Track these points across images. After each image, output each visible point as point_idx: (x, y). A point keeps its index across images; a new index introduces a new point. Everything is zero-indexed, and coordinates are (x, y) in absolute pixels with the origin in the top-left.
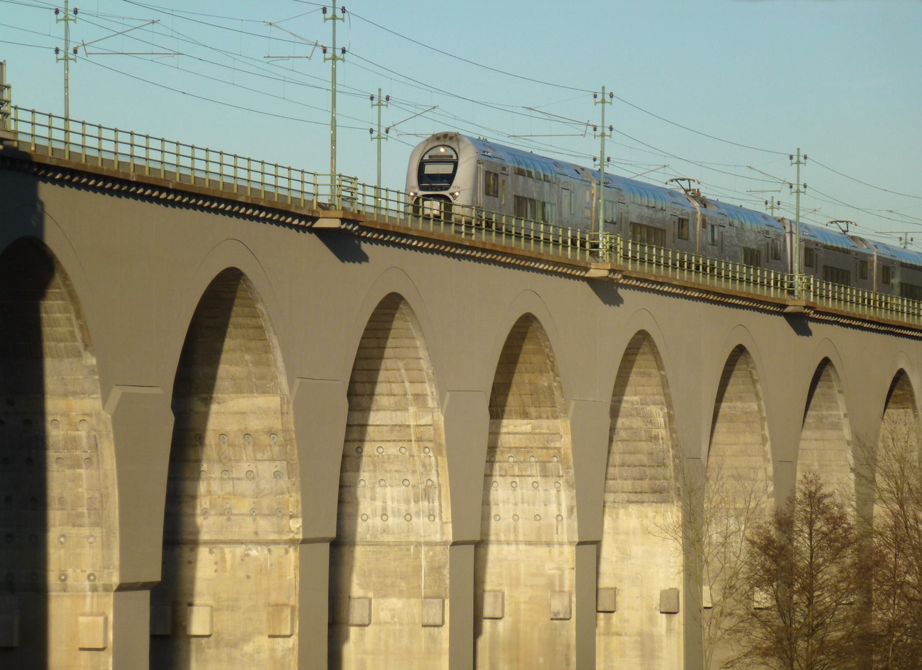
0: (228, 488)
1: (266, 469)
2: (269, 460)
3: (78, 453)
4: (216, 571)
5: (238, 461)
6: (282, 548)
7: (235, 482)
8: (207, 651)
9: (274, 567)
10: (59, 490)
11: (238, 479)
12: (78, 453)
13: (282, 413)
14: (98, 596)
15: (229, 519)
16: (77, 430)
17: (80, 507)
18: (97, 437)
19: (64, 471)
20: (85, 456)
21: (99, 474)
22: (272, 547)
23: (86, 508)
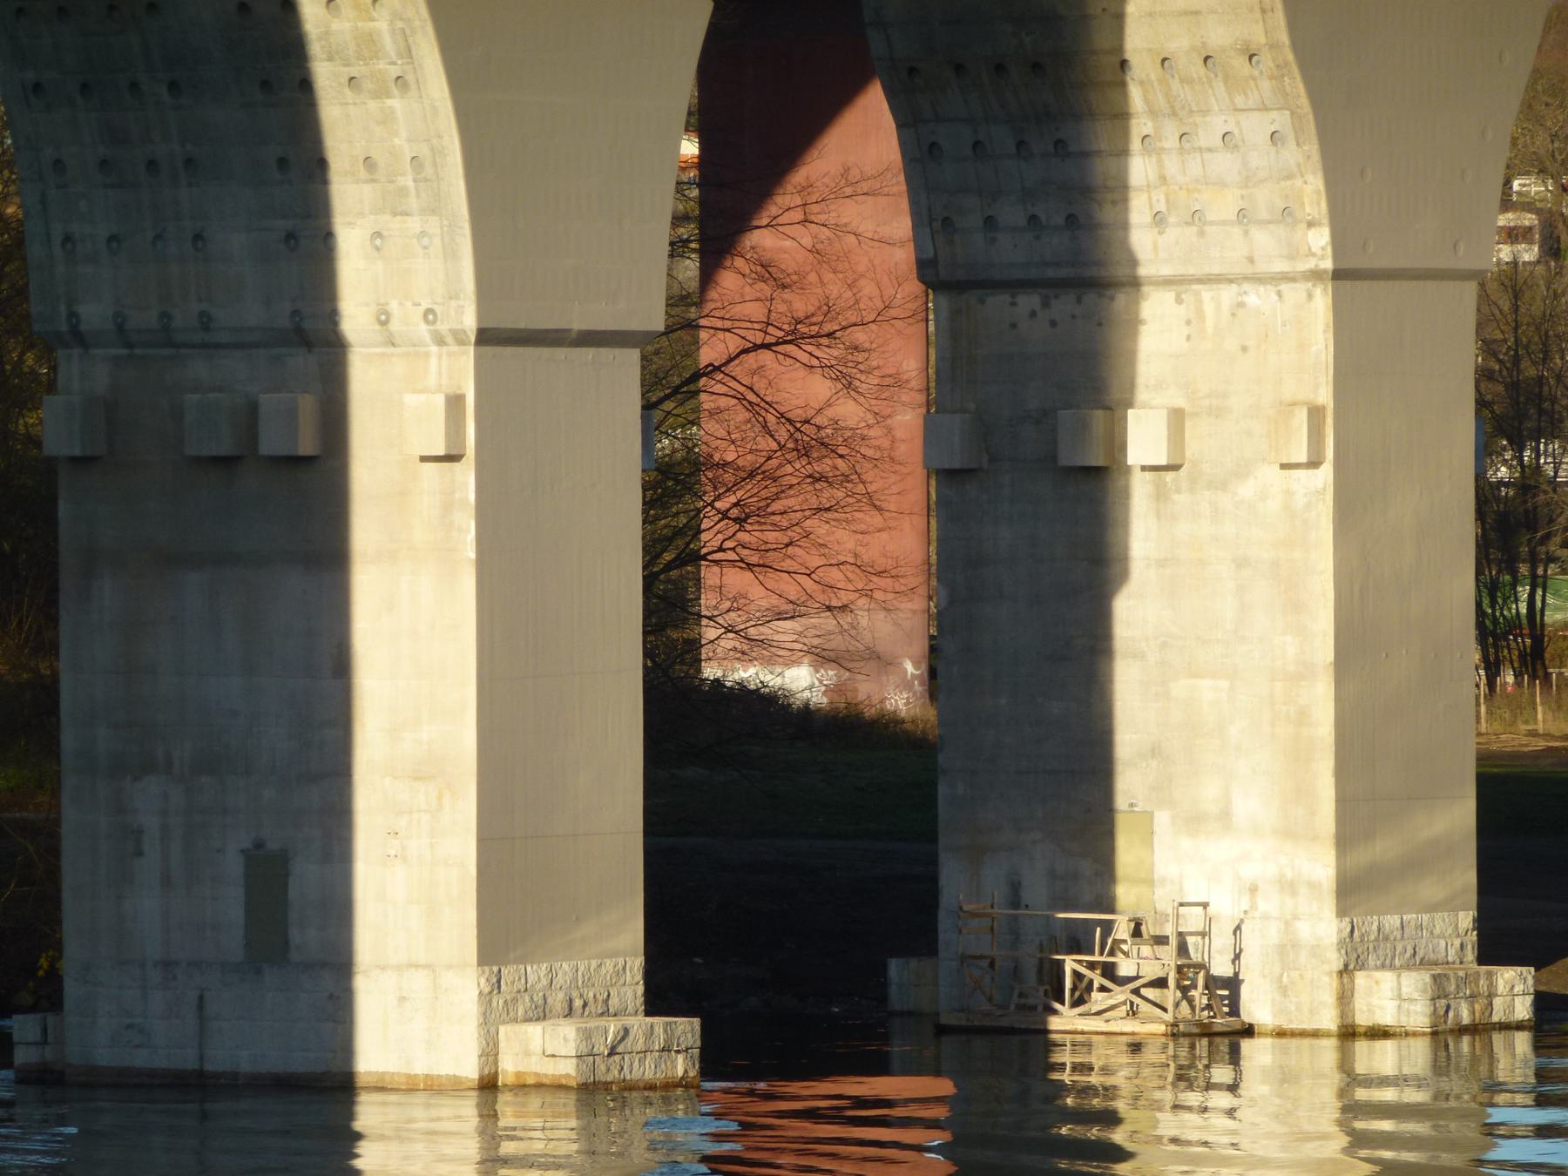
0: (1194, 166)
1: (1256, 127)
2: (1257, 109)
3: (381, 65)
4: (1188, 338)
5: (1206, 112)
6: (1302, 287)
7: (1207, 156)
8: (1176, 497)
9: (1288, 327)
10: (363, 143)
11: (1210, 150)
12: (381, 65)
13: (1263, 11)
14: (449, 354)
15: (1201, 234)
16: (373, 20)
17: (401, 175)
18: (408, 32)
19: (365, 103)
20: (394, 71)
21: (424, 108)
22: (1284, 287)
23: (410, 177)
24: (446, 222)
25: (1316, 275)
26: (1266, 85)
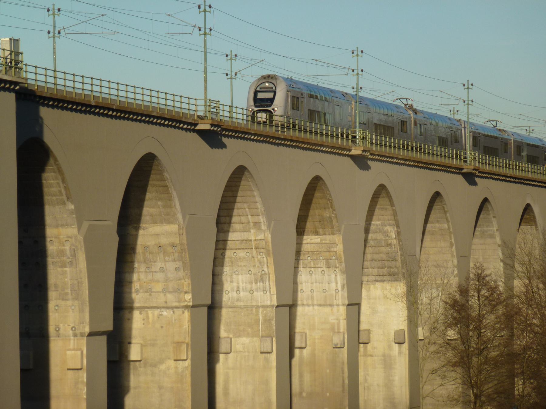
0: (150, 277)
1: (171, 266)
3: (65, 259)
4: (144, 324)
5: (155, 262)
7: (154, 273)
9: (176, 321)
10: (54, 280)
11: (155, 272)
12: (65, 259)
13: (179, 234)
15: (150, 295)
16: (64, 246)
17: (67, 289)
18: (75, 249)
20: (68, 260)
22: (175, 310)
24: (80, 302)
25: (186, 307)
26: (176, 255)
